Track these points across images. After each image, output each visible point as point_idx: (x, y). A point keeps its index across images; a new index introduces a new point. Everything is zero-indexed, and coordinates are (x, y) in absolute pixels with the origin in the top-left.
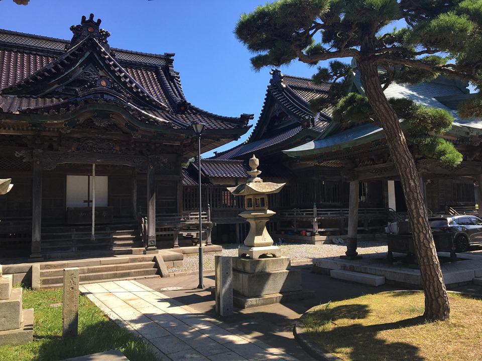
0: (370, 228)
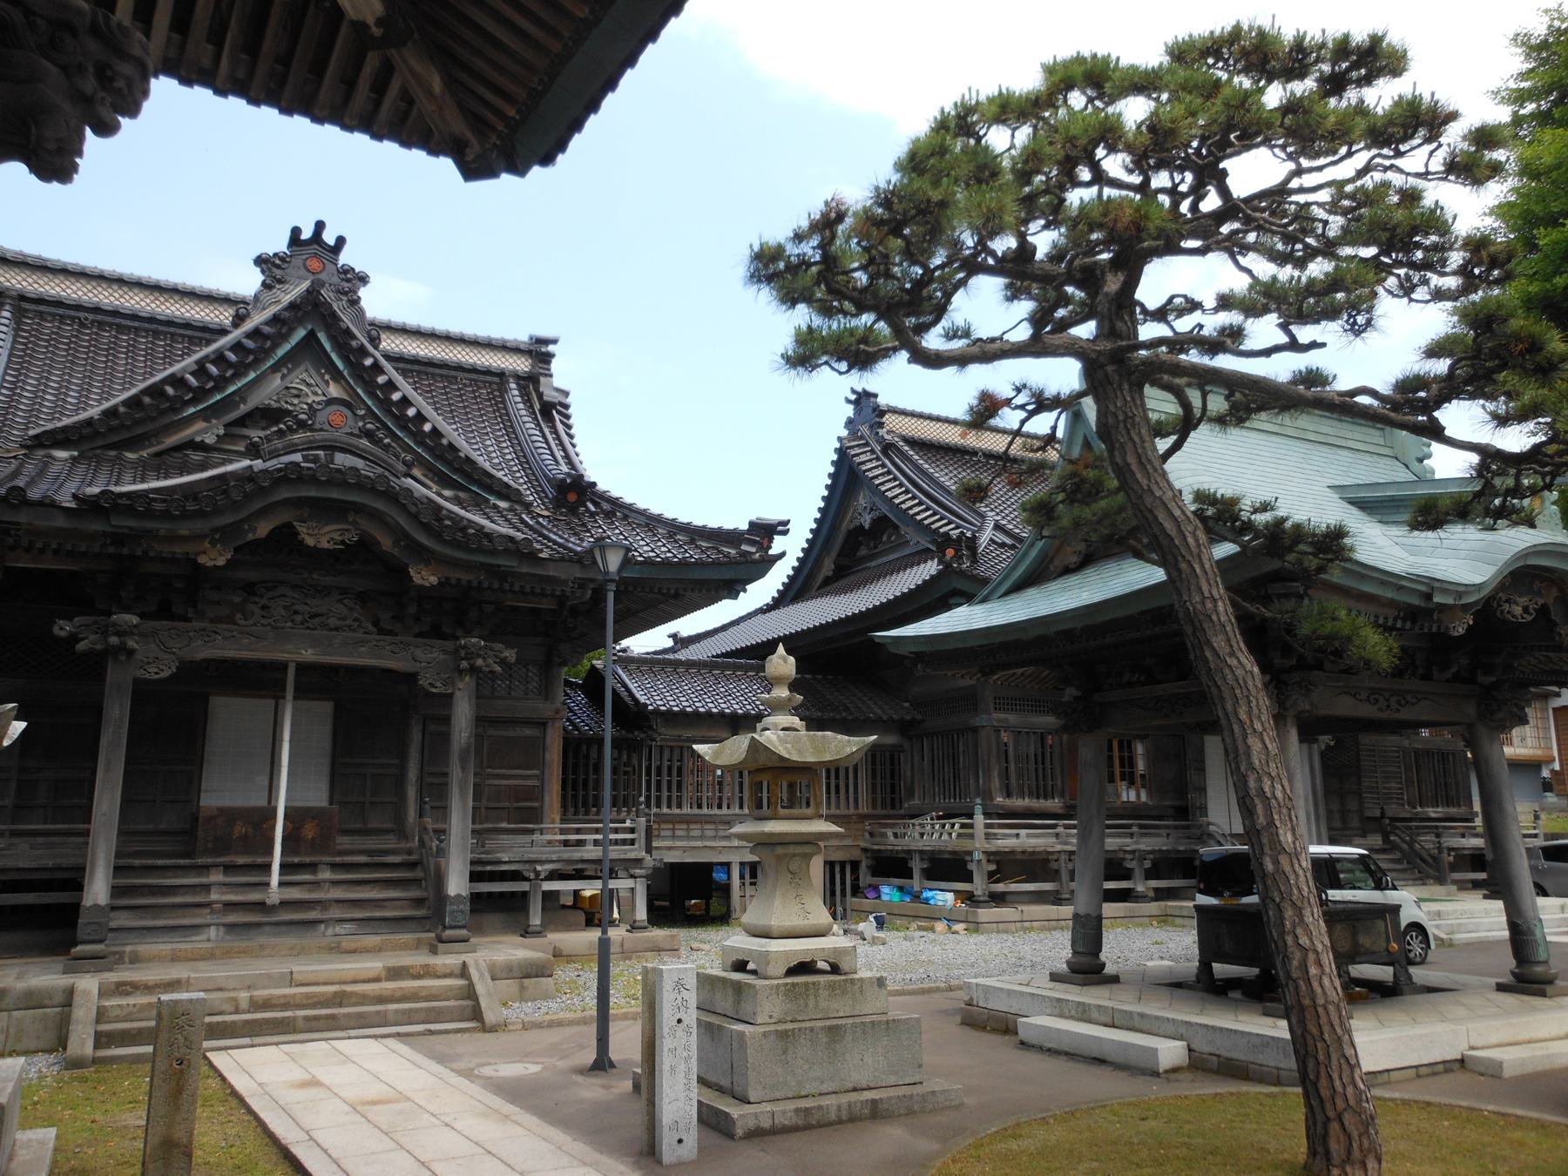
0: (1154, 883)
